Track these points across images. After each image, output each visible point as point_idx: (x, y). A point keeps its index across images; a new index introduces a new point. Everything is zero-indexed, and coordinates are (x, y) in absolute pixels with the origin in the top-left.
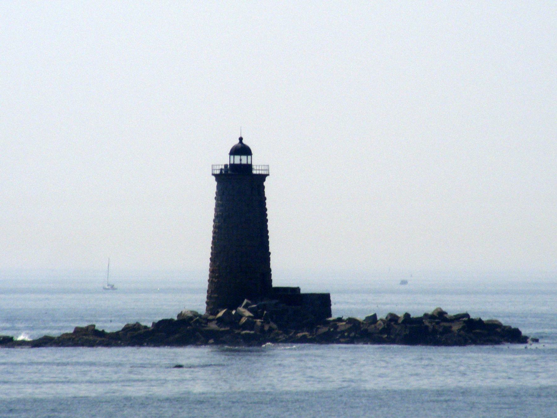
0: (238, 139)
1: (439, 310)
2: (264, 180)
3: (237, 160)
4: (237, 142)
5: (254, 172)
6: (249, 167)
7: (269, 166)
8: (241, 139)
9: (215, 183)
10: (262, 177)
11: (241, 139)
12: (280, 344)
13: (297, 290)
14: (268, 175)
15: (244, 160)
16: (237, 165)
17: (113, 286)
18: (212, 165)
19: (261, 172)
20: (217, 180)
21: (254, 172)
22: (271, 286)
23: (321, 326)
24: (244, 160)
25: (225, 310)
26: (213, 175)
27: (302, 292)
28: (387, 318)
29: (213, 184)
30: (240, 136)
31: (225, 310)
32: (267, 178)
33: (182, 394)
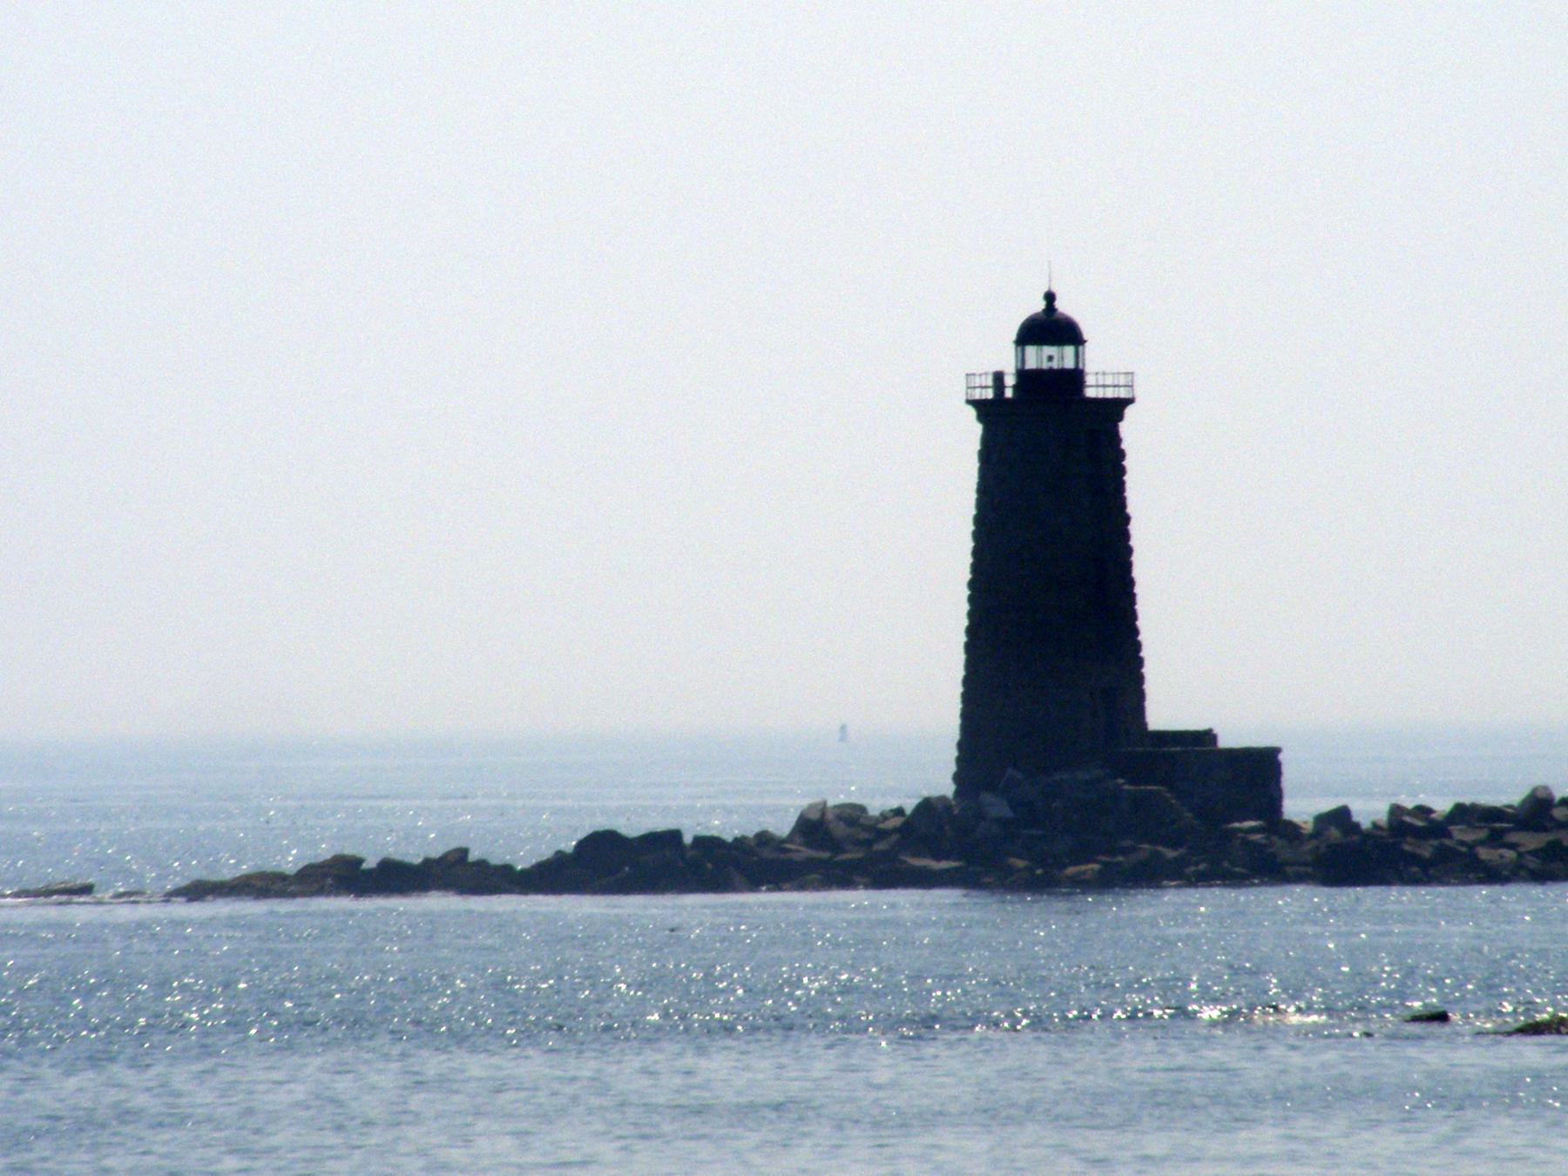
0: (1042, 295)
1: (1541, 794)
2: (1120, 417)
3: (1037, 358)
4: (1039, 306)
5: (1090, 393)
6: (1076, 377)
7: (967, 375)
8: (1050, 297)
9: (977, 429)
10: (1115, 408)
11: (1050, 297)
12: (1060, 898)
13: (1205, 738)
14: (1130, 401)
15: (1063, 357)
16: (1032, 372)
17: (843, 728)
18: (1132, 373)
19: (1110, 394)
20: (982, 417)
21: (1090, 393)
22: (1144, 724)
23: (1260, 841)
24: (1063, 357)
25: (1231, 826)
26: (971, 402)
27: (1224, 742)
28: (884, 817)
29: (972, 431)
30: (1046, 290)
31: (1231, 826)
32: (1129, 412)
33: (1420, 1038)
